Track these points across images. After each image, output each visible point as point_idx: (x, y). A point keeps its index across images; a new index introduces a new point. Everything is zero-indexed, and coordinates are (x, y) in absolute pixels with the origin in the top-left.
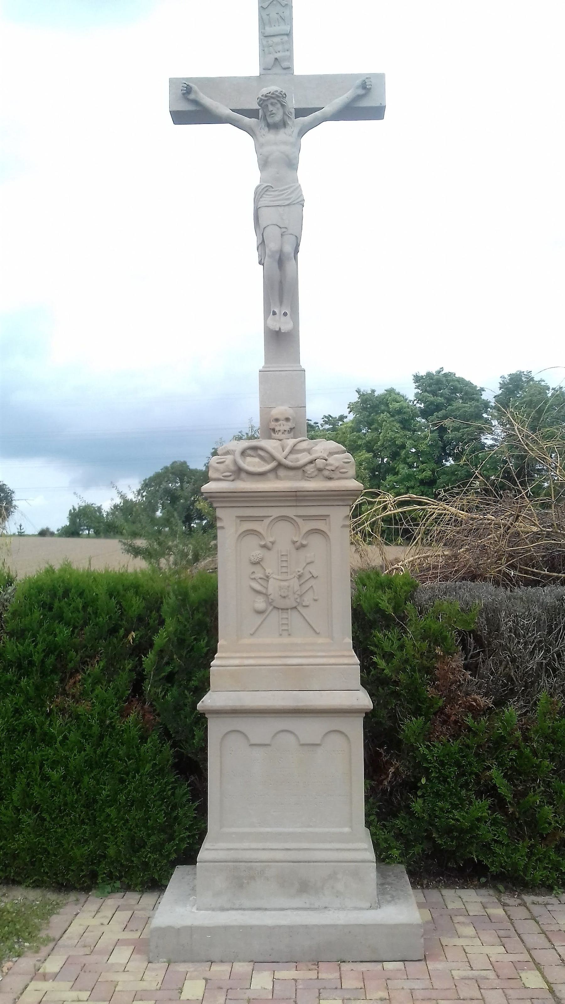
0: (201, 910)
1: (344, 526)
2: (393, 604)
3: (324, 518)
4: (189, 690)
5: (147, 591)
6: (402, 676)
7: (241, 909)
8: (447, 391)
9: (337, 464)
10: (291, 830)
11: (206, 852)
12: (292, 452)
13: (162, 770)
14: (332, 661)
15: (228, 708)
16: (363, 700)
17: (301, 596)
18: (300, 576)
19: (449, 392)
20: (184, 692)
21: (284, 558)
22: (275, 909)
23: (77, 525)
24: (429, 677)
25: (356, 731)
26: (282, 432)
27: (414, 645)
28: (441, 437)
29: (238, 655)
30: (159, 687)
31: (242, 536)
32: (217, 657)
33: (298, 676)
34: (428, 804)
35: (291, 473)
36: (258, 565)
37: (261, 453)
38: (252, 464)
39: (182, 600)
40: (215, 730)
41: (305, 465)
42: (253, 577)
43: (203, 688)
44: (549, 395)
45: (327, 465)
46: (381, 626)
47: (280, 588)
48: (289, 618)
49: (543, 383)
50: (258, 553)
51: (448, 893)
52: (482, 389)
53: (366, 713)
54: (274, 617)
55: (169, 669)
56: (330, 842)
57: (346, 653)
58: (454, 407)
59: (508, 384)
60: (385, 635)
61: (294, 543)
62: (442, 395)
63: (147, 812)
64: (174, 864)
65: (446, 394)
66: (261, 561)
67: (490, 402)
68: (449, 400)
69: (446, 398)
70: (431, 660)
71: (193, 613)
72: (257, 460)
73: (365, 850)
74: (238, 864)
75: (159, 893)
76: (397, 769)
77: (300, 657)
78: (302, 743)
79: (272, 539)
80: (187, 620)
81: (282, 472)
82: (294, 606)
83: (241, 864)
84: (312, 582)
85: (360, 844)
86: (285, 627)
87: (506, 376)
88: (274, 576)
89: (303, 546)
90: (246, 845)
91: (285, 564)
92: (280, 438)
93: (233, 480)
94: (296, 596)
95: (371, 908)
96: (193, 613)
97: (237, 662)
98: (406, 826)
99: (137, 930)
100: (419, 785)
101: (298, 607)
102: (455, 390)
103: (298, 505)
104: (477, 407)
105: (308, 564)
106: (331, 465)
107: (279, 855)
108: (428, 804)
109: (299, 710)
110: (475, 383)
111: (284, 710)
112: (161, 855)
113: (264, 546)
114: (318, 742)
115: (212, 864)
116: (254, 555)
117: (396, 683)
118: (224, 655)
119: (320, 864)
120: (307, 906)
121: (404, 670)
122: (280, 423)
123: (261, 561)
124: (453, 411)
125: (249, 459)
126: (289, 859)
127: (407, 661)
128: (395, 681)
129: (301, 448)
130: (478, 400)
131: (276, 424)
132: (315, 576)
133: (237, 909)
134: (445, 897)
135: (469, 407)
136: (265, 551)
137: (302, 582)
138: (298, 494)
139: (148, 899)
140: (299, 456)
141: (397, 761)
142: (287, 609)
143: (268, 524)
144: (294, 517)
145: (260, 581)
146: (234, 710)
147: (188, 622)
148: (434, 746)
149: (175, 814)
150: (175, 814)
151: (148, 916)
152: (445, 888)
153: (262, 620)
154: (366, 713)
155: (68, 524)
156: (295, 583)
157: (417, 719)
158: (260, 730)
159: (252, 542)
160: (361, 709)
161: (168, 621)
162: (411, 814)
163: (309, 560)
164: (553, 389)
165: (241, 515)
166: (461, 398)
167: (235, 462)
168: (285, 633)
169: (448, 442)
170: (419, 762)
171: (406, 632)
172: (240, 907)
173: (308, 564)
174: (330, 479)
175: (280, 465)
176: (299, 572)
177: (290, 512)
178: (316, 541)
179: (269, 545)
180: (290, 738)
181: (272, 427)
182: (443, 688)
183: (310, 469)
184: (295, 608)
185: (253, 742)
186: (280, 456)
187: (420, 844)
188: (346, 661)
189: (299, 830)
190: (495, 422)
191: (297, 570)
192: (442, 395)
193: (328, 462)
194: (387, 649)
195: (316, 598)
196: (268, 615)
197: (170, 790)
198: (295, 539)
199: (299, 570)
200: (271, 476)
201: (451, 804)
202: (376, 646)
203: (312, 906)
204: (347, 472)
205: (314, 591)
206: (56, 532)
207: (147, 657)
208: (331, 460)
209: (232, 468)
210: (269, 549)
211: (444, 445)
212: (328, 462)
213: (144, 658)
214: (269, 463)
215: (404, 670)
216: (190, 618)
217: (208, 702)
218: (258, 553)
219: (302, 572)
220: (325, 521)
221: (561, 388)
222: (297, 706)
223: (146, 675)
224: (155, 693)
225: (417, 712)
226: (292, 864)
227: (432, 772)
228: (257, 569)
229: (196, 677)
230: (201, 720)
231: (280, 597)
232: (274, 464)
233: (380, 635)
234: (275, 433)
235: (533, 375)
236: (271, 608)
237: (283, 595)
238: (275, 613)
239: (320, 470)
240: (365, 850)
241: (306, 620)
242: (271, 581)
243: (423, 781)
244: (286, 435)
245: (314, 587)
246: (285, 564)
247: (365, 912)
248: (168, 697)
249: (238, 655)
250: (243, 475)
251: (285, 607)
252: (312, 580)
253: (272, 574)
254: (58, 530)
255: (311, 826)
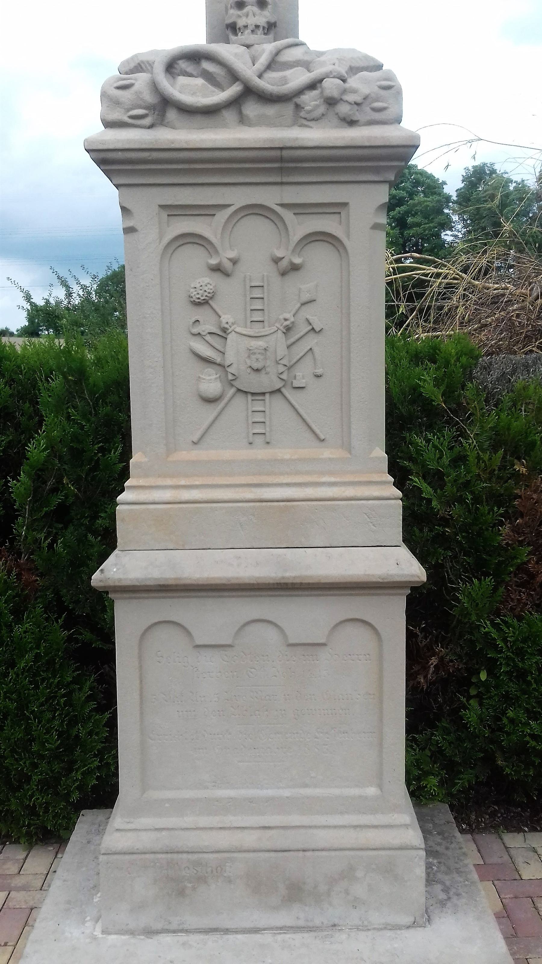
0: (109, 934)
1: (376, 227)
2: (442, 388)
3: (338, 208)
4: (95, 533)
5: (19, 367)
6: (456, 510)
7: (182, 931)
8: (408, 185)
9: (365, 90)
10: (270, 793)
11: (118, 835)
12: (271, 66)
13: (50, 663)
14: (350, 492)
15: (152, 583)
16: (410, 568)
17: (290, 368)
18: (288, 330)
19: (411, 186)
20: (86, 536)
21: (257, 293)
22: (244, 931)
23: (35, 325)
24: (502, 511)
25: (392, 620)
26: (251, 28)
27: (478, 458)
28: (402, 234)
29: (169, 482)
30: (42, 530)
31: (170, 252)
32: (128, 487)
33: (283, 521)
34: (487, 709)
35: (270, 110)
36: (206, 307)
37: (206, 65)
38: (190, 90)
39: (75, 382)
40: (127, 623)
41: (300, 92)
42: (195, 330)
43: (108, 542)
44: (511, 188)
45: (345, 91)
46: (420, 425)
47: (250, 352)
48: (267, 411)
49: (505, 176)
50: (205, 282)
51: (514, 840)
52: (444, 183)
53: (412, 589)
54: (239, 408)
55: (56, 500)
56: (342, 813)
57: (376, 478)
58: (416, 201)
59: (471, 177)
60: (428, 441)
61: (276, 261)
62: (404, 189)
63: (28, 730)
64: (79, 807)
65: (408, 188)
66: (211, 298)
67: (451, 196)
68: (411, 195)
69: (407, 192)
70: (506, 482)
71: (96, 405)
72: (200, 81)
73: (406, 826)
74: (175, 856)
75: (56, 846)
76: (441, 659)
77: (288, 485)
78: (291, 641)
79: (232, 254)
80: (84, 416)
81: (251, 109)
82: (277, 387)
83: (180, 856)
84: (311, 341)
85: (396, 815)
86: (259, 429)
87: (471, 168)
88: (238, 329)
89: (295, 268)
90: (189, 820)
91: (258, 305)
92: (248, 42)
93: (151, 127)
94: (281, 369)
95: (414, 925)
96: (96, 405)
97: (167, 495)
98: (450, 743)
99: (6, 944)
100: (474, 680)
101: (283, 390)
102: (417, 183)
103: (285, 180)
104: (439, 201)
105: (303, 304)
106: (354, 91)
107: (250, 839)
108: (487, 709)
109: (286, 584)
110: (437, 177)
111: (258, 584)
112: (57, 794)
113: (217, 269)
114: (323, 641)
115: (127, 857)
116: (198, 286)
117: (445, 522)
118: (142, 482)
119: (324, 853)
120: (301, 923)
121: (461, 500)
122: (246, 10)
123: (211, 298)
124: (415, 205)
125: (182, 80)
126: (269, 845)
127: (467, 485)
128: (443, 518)
129: (290, 59)
130: (439, 194)
131: (239, 13)
132: (317, 329)
133: (174, 932)
134: (513, 852)
135: (431, 201)
136: (217, 276)
137: (292, 340)
138: (285, 153)
139: (37, 861)
140: (288, 73)
141: (442, 647)
142: (264, 394)
143: (223, 221)
144: (278, 209)
145: (208, 338)
146: (164, 586)
147: (88, 421)
148: (505, 622)
149: (74, 732)
150: (74, 732)
151: (31, 904)
152: (509, 831)
153: (215, 413)
154: (412, 589)
155: (27, 324)
156: (278, 343)
157: (479, 580)
158: (213, 620)
159: (193, 259)
160: (406, 582)
161: (49, 419)
162: (461, 725)
163: (305, 297)
164: (516, 182)
165: (169, 203)
166: (423, 192)
167: (155, 87)
168: (259, 440)
169: (408, 239)
170: (480, 649)
171: (463, 434)
172: (181, 927)
173: (303, 304)
174: (352, 123)
175: (249, 92)
176: (286, 320)
177: (269, 197)
178: (319, 257)
179: (228, 265)
180: (270, 635)
181: (229, 21)
182: (527, 530)
183: (310, 100)
184: (279, 391)
185: (199, 642)
186: (248, 71)
187: (472, 768)
188: (376, 491)
189: (287, 793)
190: (455, 218)
191: (281, 317)
192: (404, 189)
193: (347, 85)
194: (432, 466)
195: (319, 371)
196: (227, 404)
197: (63, 696)
198: (279, 254)
199: (287, 316)
200: (229, 115)
201: (527, 711)
202: (410, 459)
203: (310, 924)
204: (385, 109)
205: (315, 359)
206: (16, 333)
207: (18, 481)
208: (353, 82)
209: (149, 98)
210: (227, 275)
211: (404, 242)
212: (347, 85)
213: (12, 483)
214: (223, 90)
215: (461, 500)
216: (90, 413)
217: (115, 570)
218: (205, 282)
219: (292, 319)
220: (337, 216)
221: (523, 181)
222: (283, 578)
223: (17, 510)
224: (36, 541)
225: (479, 570)
226: (273, 854)
227: (501, 664)
228: (202, 314)
229: (106, 512)
230: (100, 605)
231: (249, 370)
232: (235, 89)
233: (420, 441)
234: (236, 35)
235: (496, 167)
236: (233, 390)
237: (256, 366)
238: (240, 401)
239: (331, 102)
240: (406, 826)
241: (301, 416)
242: (232, 337)
243: (483, 676)
244: (259, 36)
245: (316, 350)
246: (258, 305)
247: (405, 933)
248: (59, 547)
249: (169, 482)
250: (172, 115)
251: (257, 393)
252: (312, 335)
253: (233, 324)
254: (17, 331)
255: (306, 786)
